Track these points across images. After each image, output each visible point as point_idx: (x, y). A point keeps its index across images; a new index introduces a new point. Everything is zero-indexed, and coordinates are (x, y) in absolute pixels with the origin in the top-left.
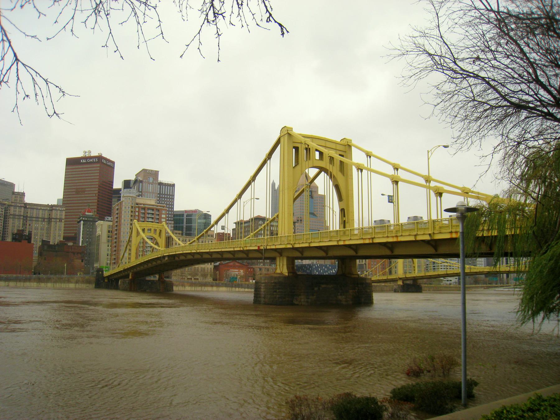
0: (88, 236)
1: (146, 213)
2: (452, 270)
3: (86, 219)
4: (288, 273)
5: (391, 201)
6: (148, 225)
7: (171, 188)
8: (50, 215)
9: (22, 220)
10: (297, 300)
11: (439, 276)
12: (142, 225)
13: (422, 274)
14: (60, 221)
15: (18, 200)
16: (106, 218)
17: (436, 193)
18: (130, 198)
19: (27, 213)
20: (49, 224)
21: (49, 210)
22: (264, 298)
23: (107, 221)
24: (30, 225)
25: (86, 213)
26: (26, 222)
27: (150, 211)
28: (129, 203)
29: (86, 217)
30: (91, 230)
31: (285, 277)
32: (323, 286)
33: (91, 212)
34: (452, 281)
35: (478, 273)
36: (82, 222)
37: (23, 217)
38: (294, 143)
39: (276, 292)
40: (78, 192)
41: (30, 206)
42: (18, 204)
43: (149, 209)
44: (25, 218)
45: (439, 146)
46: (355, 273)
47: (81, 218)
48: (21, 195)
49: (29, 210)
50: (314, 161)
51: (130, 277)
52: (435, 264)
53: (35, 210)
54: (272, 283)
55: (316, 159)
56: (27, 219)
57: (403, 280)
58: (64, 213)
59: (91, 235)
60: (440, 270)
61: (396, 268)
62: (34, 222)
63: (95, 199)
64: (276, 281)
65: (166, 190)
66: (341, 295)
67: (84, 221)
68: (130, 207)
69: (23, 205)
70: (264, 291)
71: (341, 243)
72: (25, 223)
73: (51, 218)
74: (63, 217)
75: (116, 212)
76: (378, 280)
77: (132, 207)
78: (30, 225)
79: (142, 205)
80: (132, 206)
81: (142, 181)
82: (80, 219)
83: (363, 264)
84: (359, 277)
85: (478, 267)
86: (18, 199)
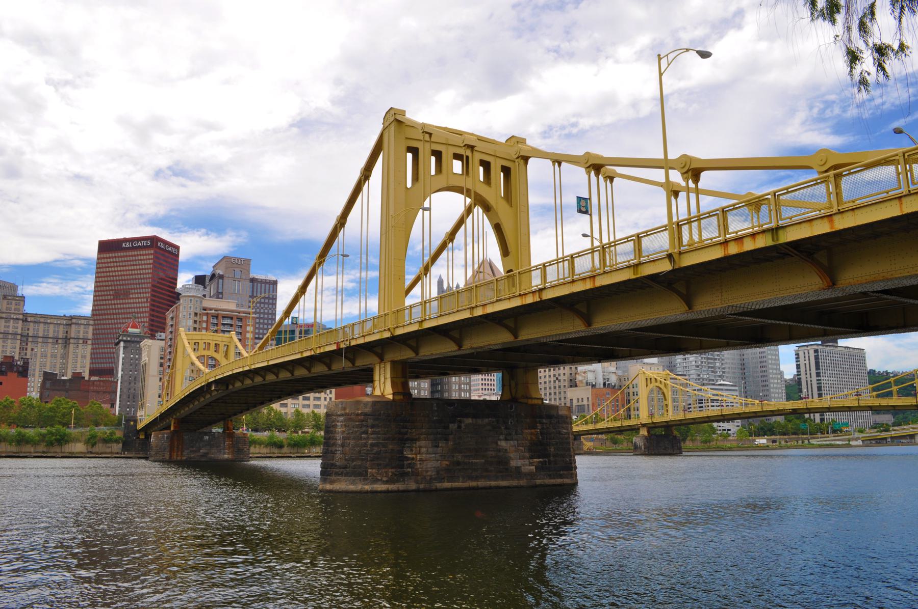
0: (131, 367)
1: (219, 324)
3: (129, 339)
4: (394, 394)
5: (584, 209)
7: (271, 286)
8: (67, 332)
9: (18, 342)
10: (412, 450)
11: (709, 420)
12: (194, 337)
13: (680, 416)
14: (83, 342)
15: (13, 309)
16: (158, 335)
17: (686, 172)
18: (192, 299)
19: (28, 329)
20: (65, 347)
21: (67, 325)
22: (343, 446)
23: (158, 339)
24: (32, 350)
25: (130, 330)
26: (27, 344)
28: (190, 308)
29: (129, 336)
30: (137, 356)
31: (388, 403)
32: (469, 421)
33: (137, 328)
34: (732, 430)
35: (775, 413)
37: (22, 336)
38: (408, 140)
39: (366, 432)
41: (32, 319)
42: (12, 316)
43: (224, 317)
44: (25, 338)
45: (687, 50)
47: (120, 338)
48: (17, 300)
49: (32, 324)
52: (702, 403)
53: (42, 325)
54: (358, 415)
55: (455, 171)
56: (27, 339)
57: (651, 427)
58: (91, 328)
60: (711, 408)
61: (638, 410)
62: (50, 345)
63: (146, 307)
64: (368, 410)
66: (506, 439)
67: (125, 341)
68: (193, 314)
69: (21, 317)
71: (479, 312)
72: (25, 347)
73: (68, 337)
74: (90, 336)
76: (607, 428)
77: (196, 314)
78: (32, 350)
79: (213, 312)
80: (196, 312)
81: (223, 275)
84: (543, 403)
85: (773, 402)
86: (13, 307)
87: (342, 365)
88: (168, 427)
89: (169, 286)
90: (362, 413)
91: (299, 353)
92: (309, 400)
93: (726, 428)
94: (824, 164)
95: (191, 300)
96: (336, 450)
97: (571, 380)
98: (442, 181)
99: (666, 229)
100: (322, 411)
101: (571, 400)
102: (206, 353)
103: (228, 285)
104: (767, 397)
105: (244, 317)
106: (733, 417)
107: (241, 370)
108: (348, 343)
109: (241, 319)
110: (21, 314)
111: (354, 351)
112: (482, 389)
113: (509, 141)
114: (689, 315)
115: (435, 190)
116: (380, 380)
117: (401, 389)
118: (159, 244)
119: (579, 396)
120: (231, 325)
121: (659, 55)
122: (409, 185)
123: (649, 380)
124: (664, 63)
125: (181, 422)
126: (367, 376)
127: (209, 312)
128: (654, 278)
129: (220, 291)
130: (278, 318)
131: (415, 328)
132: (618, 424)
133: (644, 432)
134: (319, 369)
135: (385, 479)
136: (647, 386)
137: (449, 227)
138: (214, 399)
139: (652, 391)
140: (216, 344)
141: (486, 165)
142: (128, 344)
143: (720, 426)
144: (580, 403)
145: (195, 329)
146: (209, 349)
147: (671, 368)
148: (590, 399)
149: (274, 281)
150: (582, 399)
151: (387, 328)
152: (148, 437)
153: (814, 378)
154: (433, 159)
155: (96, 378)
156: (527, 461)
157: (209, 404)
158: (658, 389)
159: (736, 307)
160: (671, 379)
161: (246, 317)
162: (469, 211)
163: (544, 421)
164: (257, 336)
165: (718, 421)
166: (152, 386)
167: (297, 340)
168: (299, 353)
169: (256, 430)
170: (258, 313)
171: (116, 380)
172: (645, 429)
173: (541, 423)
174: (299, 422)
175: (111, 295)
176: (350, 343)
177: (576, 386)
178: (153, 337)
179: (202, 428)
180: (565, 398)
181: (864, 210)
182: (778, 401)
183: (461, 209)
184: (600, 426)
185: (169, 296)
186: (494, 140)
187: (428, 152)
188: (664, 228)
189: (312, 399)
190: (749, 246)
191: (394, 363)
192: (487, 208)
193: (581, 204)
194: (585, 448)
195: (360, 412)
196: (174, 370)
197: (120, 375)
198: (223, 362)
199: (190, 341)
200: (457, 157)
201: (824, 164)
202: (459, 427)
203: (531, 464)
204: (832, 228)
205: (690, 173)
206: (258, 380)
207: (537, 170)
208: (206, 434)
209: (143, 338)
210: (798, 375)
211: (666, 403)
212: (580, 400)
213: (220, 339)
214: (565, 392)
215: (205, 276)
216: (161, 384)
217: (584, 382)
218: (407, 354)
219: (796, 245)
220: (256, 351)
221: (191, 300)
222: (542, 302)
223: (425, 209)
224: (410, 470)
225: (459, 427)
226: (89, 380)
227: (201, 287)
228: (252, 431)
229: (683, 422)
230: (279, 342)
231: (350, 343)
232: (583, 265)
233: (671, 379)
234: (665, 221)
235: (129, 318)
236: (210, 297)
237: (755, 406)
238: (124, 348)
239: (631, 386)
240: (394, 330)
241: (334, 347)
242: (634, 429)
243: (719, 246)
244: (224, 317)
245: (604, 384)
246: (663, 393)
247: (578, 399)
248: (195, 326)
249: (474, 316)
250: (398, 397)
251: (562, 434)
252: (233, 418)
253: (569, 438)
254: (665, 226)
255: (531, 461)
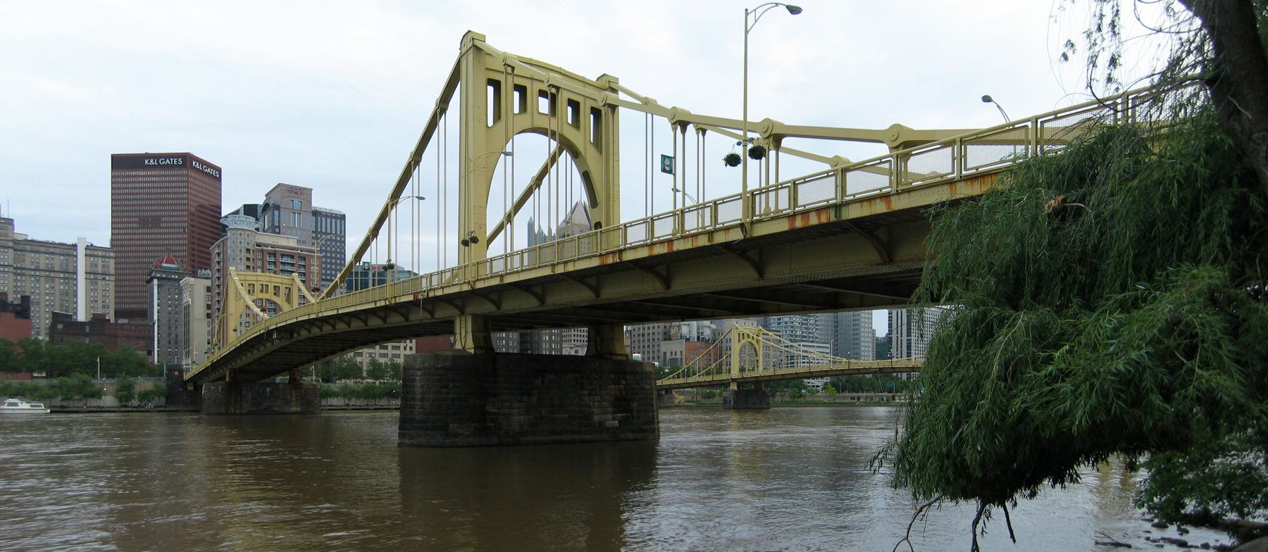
1: (278, 263)
2: (820, 364)
4: (475, 349)
5: (668, 169)
6: (273, 280)
11: (799, 377)
13: (770, 372)
17: (768, 138)
18: (242, 232)
22: (422, 400)
27: (285, 260)
28: (241, 242)
29: (164, 272)
30: (176, 296)
31: (470, 356)
36: (155, 282)
40: (145, 222)
43: (283, 255)
46: (618, 351)
47: (153, 274)
50: (536, 116)
51: (227, 379)
54: (437, 369)
57: (741, 383)
59: (176, 307)
65: (329, 226)
67: (159, 279)
70: (422, 387)
71: (560, 270)
74: (112, 271)
75: (216, 260)
77: (248, 250)
79: (270, 248)
80: (248, 248)
82: (150, 275)
83: (677, 359)
84: (627, 359)
87: (419, 316)
88: (223, 378)
89: (213, 216)
90: (441, 367)
91: (372, 302)
92: (387, 349)
93: (816, 385)
94: (896, 140)
95: (241, 234)
96: (415, 405)
97: (665, 333)
98: (526, 121)
99: (741, 198)
100: (401, 361)
101: (665, 353)
102: (264, 296)
103: (287, 219)
104: (857, 356)
105: (307, 255)
106: (822, 374)
107: (306, 318)
108: (426, 294)
109: (304, 259)
110: (11, 241)
111: (432, 303)
112: (574, 340)
113: (600, 80)
114: (761, 282)
115: (519, 131)
116: (461, 334)
117: (483, 343)
118: (194, 163)
119: (674, 348)
120: (292, 265)
121: (746, 10)
122: (490, 123)
123: (741, 335)
124: (751, 18)
125: (235, 372)
126: (447, 327)
127: (264, 248)
128: (727, 246)
129: (276, 224)
130: (347, 263)
131: (496, 282)
132: (709, 378)
133: (734, 387)
134: (395, 320)
135: (467, 433)
136: (739, 341)
137: (535, 172)
138: (277, 348)
139: (744, 347)
140: (275, 287)
141: (575, 105)
142: (163, 282)
143: (809, 383)
144: (674, 356)
145: (248, 267)
146: (267, 292)
147: (766, 326)
148: (684, 353)
149: (341, 215)
150: (676, 352)
151: (466, 281)
152: (198, 388)
153: (905, 338)
154: (516, 94)
155: (125, 321)
156: (610, 416)
157: (271, 353)
158: (750, 345)
159: (803, 277)
160: (763, 334)
161: (310, 255)
162: (553, 159)
163: (628, 377)
164: (324, 277)
165: (808, 378)
166: (200, 330)
167: (371, 288)
168: (372, 302)
169: (327, 380)
170: (324, 251)
171: (151, 324)
172: (735, 384)
173: (624, 379)
174: (376, 370)
175: (135, 222)
176: (428, 294)
177: (670, 340)
178: (194, 275)
179: (264, 378)
180: (658, 351)
181: (918, 193)
182: (867, 360)
183: (544, 158)
184: (691, 380)
185: (213, 233)
186: (584, 78)
187: (510, 86)
188: (740, 196)
189: (390, 347)
190: (814, 220)
191: (475, 317)
192: (575, 154)
193: (665, 162)
194: (676, 402)
195: (439, 366)
196: (225, 315)
197: (156, 317)
198: (286, 307)
199: (243, 283)
200: (543, 94)
201: (896, 140)
202: (543, 382)
203: (614, 419)
204: (889, 208)
205: (771, 139)
206: (327, 329)
207: (629, 122)
208: (268, 385)
209: (182, 276)
210: (889, 334)
211: (757, 358)
212: (674, 353)
213: (280, 281)
214: (659, 345)
215: (257, 205)
216: (210, 329)
217: (679, 335)
218: (488, 308)
219: (857, 223)
220: (323, 298)
221: (241, 234)
222: (622, 263)
223: (506, 154)
224: (492, 424)
225: (543, 382)
226: (116, 324)
227: (252, 219)
228: (323, 380)
229: (772, 378)
230: (349, 288)
231: (428, 294)
232: (664, 229)
233: (763, 334)
234: (741, 191)
235: (161, 251)
236: (264, 231)
237: (843, 364)
238: (159, 286)
239: (724, 341)
240: (474, 285)
241: (411, 298)
242: (724, 384)
243: (786, 219)
244: (283, 255)
245: (698, 338)
246: (755, 349)
247: (672, 352)
248: (248, 263)
249: (556, 273)
250: (478, 352)
251: (646, 390)
252: (300, 368)
253: (653, 393)
254: (741, 195)
255: (614, 416)
